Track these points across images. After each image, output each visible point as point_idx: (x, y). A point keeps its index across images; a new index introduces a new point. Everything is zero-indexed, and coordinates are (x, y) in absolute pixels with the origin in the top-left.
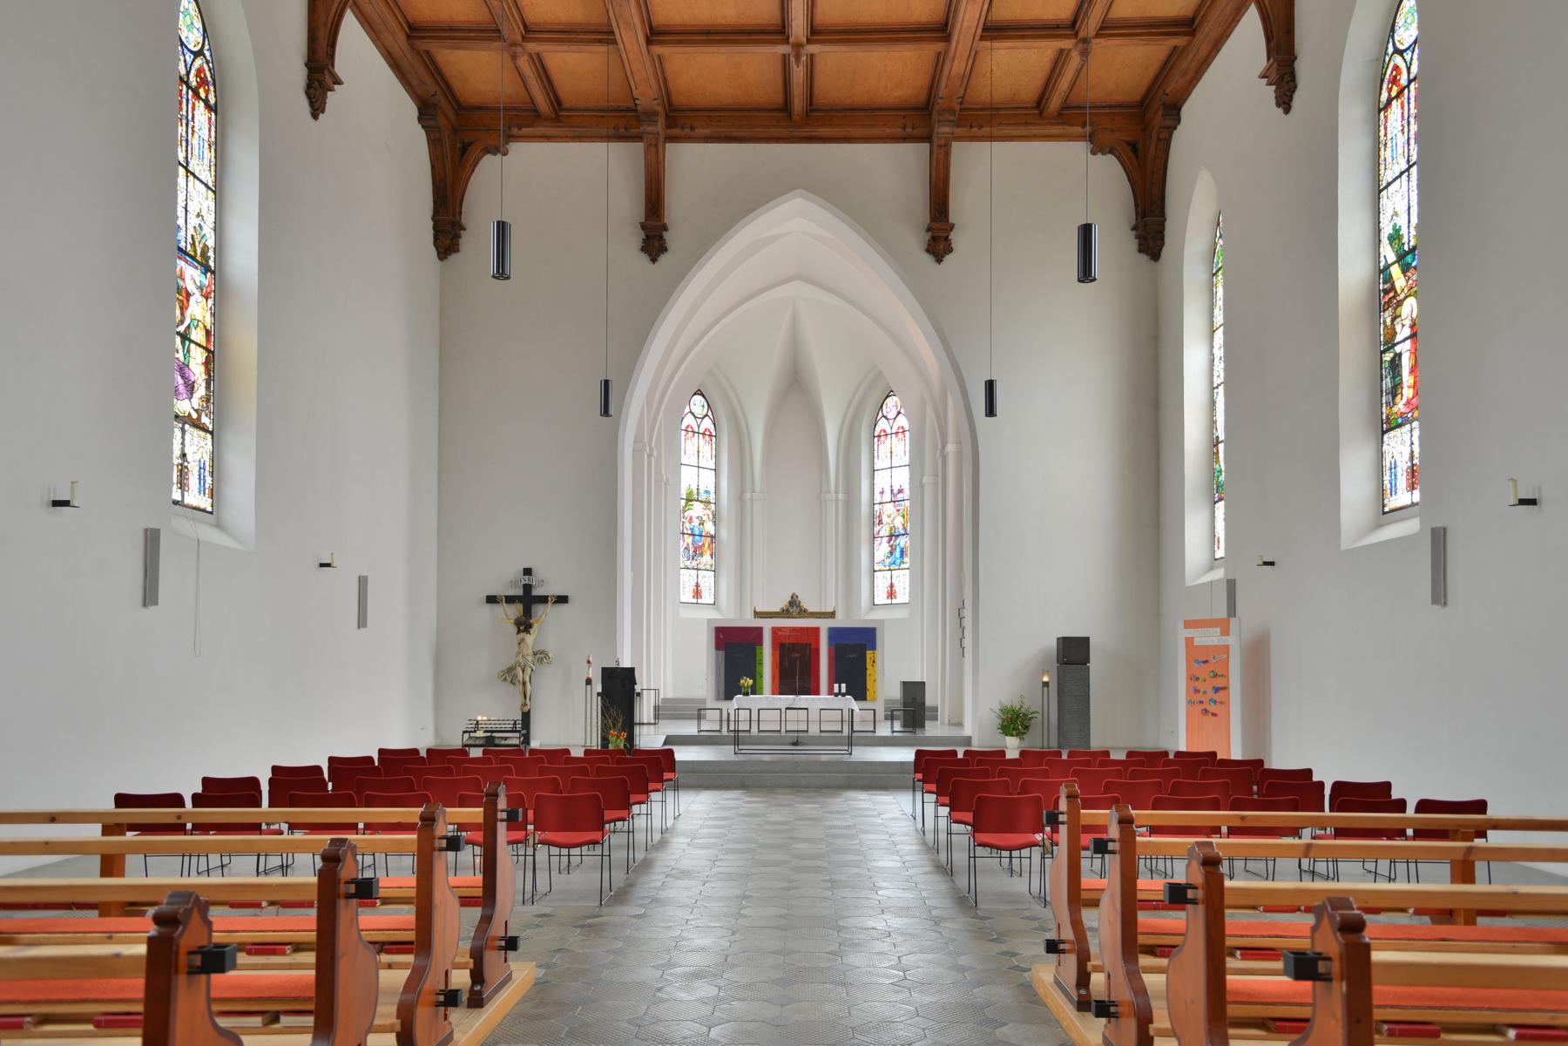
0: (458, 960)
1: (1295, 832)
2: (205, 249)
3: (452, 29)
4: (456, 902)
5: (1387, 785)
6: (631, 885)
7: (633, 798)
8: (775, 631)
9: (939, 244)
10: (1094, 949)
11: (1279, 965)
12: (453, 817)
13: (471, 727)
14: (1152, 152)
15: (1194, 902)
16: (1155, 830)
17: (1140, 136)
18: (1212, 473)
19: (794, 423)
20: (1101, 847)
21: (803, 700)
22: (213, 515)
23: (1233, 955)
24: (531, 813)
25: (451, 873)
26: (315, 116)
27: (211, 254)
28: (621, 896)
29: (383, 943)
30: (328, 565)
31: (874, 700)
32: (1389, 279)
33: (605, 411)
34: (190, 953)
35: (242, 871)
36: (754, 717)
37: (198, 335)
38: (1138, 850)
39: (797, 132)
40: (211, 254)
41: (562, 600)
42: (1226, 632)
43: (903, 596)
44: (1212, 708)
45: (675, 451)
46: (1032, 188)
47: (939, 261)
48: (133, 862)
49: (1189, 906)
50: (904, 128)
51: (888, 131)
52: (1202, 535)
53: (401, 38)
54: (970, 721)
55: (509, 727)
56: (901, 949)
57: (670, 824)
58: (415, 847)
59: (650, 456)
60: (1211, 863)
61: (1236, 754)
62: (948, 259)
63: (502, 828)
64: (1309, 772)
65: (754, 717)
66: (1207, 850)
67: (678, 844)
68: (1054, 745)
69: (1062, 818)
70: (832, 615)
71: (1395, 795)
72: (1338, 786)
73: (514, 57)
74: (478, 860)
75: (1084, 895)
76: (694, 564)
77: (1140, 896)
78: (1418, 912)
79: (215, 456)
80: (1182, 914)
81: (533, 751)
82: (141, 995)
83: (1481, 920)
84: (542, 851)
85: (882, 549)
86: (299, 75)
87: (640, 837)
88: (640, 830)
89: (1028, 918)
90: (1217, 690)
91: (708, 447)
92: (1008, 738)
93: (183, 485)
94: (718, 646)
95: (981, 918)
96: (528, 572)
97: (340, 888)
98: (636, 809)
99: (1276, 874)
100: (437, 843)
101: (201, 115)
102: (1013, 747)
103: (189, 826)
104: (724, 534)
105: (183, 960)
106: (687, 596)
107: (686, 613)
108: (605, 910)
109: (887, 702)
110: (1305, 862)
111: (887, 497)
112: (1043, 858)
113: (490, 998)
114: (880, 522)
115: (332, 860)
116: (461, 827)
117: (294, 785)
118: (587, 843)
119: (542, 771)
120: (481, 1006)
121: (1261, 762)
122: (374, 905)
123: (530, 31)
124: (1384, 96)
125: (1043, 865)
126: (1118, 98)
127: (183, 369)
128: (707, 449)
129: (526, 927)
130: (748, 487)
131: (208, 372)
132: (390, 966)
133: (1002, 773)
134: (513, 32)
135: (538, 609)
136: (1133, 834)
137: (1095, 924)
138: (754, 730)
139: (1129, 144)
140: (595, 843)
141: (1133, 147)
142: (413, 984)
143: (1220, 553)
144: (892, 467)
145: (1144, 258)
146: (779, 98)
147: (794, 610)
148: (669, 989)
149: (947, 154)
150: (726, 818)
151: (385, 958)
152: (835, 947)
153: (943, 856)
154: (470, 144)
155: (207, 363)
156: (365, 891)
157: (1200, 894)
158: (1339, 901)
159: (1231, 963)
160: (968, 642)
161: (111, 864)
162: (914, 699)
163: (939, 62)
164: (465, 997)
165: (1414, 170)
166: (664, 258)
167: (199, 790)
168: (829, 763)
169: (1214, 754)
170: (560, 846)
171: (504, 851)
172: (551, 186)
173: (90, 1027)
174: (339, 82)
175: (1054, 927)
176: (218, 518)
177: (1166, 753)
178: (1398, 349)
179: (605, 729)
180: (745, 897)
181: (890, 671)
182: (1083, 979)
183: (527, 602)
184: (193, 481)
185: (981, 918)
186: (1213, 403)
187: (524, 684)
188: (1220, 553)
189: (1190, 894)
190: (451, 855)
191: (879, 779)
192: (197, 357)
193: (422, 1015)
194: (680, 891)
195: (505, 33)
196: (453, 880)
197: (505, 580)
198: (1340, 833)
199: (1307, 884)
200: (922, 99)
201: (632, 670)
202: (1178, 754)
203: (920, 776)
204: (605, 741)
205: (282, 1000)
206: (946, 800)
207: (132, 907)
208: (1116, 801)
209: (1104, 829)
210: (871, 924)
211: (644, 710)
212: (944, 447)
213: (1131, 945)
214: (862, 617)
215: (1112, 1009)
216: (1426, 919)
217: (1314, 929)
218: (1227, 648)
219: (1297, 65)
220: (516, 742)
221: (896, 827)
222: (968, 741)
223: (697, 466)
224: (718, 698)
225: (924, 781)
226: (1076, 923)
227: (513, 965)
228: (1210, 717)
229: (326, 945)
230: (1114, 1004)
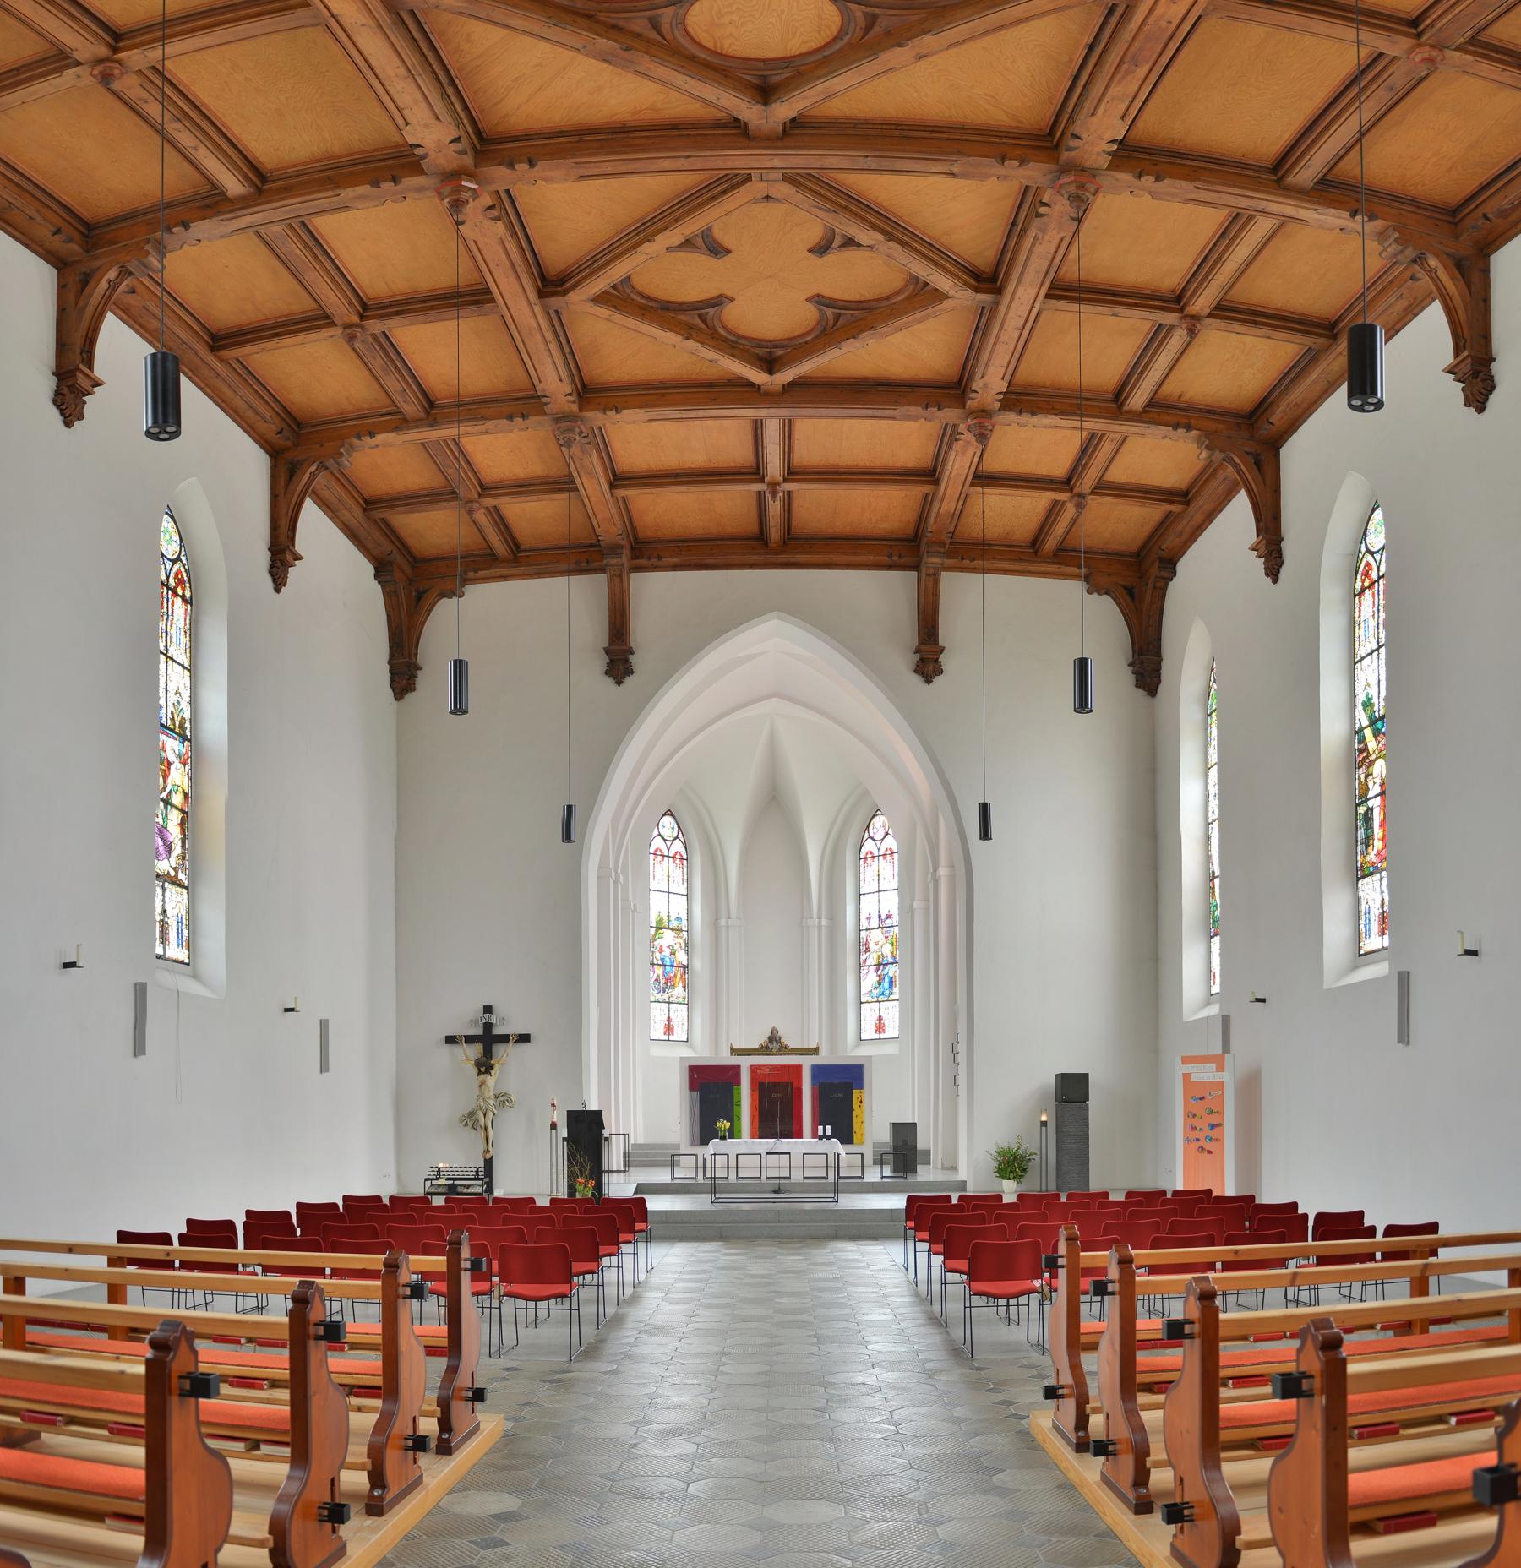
0: (425, 1407)
1: (1282, 1263)
2: (183, 720)
3: (407, 497)
4: (422, 1352)
5: (1360, 1214)
6: (602, 1341)
7: (603, 1249)
8: (754, 1069)
9: (928, 664)
10: (1093, 1390)
11: (1268, 1389)
12: (417, 1264)
13: (433, 1175)
15: (1191, 1336)
16: (1153, 1270)
19: (772, 841)
20: (1101, 1289)
21: (785, 1144)
22: (189, 966)
23: (1225, 1385)
24: (495, 1265)
25: (416, 1322)
26: (278, 590)
27: (187, 725)
28: (591, 1352)
29: (353, 1386)
31: (862, 1143)
32: (1363, 740)
34: (181, 1377)
35: (223, 1308)
36: (732, 1163)
37: (177, 799)
38: (1137, 1290)
39: (772, 558)
40: (187, 725)
41: (524, 1038)
42: (1221, 1068)
43: (892, 1030)
44: (1208, 1145)
45: (643, 875)
48: (133, 1292)
49: (1186, 1341)
50: (890, 556)
51: (872, 558)
52: (1198, 969)
54: (965, 1165)
55: (472, 1174)
56: (893, 1404)
57: (642, 1277)
58: (380, 1294)
60: (1207, 1297)
61: (1230, 1191)
62: (938, 680)
63: (466, 1278)
64: (1295, 1205)
65: (732, 1163)
66: (1204, 1285)
67: (652, 1298)
68: (1052, 1188)
69: (1061, 1261)
70: (815, 1051)
71: (1367, 1223)
72: (1320, 1217)
73: (470, 512)
74: (443, 1310)
75: (1083, 1339)
76: (666, 996)
77: (1139, 1336)
78: (1384, 1328)
79: (190, 910)
80: (1179, 1352)
81: (496, 1200)
82: (143, 1411)
83: (1433, 1329)
84: (508, 1304)
85: (869, 979)
86: (263, 558)
87: (611, 1291)
88: (610, 1284)
89: (1025, 1366)
90: (1213, 1127)
91: (679, 871)
92: (1005, 1182)
93: (164, 940)
94: (692, 1087)
95: (977, 1369)
96: (488, 1009)
97: (310, 1332)
98: (605, 1261)
99: (1267, 1302)
100: (401, 1291)
101: (179, 607)
102: (1009, 1191)
103: (177, 1264)
104: (697, 964)
105: (175, 1381)
106: (658, 1032)
107: (657, 1051)
108: (574, 1365)
109: (875, 1145)
110: (1291, 1290)
111: (875, 923)
112: (1041, 1305)
113: (458, 1447)
114: (867, 950)
115: (301, 1302)
116: (426, 1275)
117: (266, 1228)
118: (556, 1296)
119: (506, 1221)
120: (450, 1453)
121: (1252, 1198)
122: (342, 1349)
123: (485, 489)
124: (1358, 585)
125: (1041, 1313)
127: (162, 832)
128: (678, 873)
129: (493, 1380)
130: (724, 913)
131: (183, 831)
132: (359, 1409)
133: (998, 1219)
134: (469, 490)
135: (499, 1050)
136: (1133, 1274)
137: (1094, 1368)
138: (732, 1177)
139: (1125, 588)
140: (563, 1296)
141: (1130, 591)
142: (382, 1427)
143: (1216, 989)
144: (879, 891)
145: (1141, 692)
147: (775, 1046)
148: (644, 1445)
149: (937, 583)
150: (704, 1272)
151: (355, 1401)
152: (821, 1403)
153: (937, 1308)
155: (182, 824)
156: (333, 1333)
157: (1196, 1328)
158: (1321, 1322)
159: (1224, 1393)
160: (962, 1080)
161: (116, 1293)
162: (905, 1142)
163: (926, 504)
164: (433, 1444)
165: (1383, 650)
166: (629, 681)
167: (184, 1231)
168: (816, 1211)
169: (1210, 1191)
170: (527, 1299)
171: (469, 1303)
172: (515, 625)
173: (106, 1433)
175: (1053, 1374)
176: (194, 969)
177: (1164, 1193)
178: (1370, 804)
179: (572, 1177)
180: (725, 1354)
181: (877, 1116)
182: (1082, 1422)
183: (487, 1042)
184: (173, 935)
185: (977, 1369)
187: (486, 1129)
188: (1216, 989)
189: (1187, 1329)
190: (415, 1302)
191: (867, 1228)
192: (175, 817)
193: (392, 1458)
194: (654, 1348)
195: (461, 492)
196: (418, 1329)
197: (465, 1021)
198: (1322, 1260)
199: (1293, 1310)
200: (910, 530)
201: (600, 1112)
202: (1176, 1193)
203: (912, 1224)
204: (572, 1189)
205: (261, 1429)
206: (940, 1248)
207: (133, 1333)
208: (1115, 1241)
209: (1104, 1271)
210: (860, 1379)
211: (614, 1156)
212: (935, 870)
213: (1130, 1384)
214: (849, 1054)
215: (1111, 1448)
216: (1390, 1333)
217: (1299, 1350)
218: (1221, 1085)
220: (479, 1190)
221: (885, 1283)
222: (963, 1185)
223: (668, 892)
224: (692, 1143)
225: (916, 1229)
226: (1076, 1368)
227: (480, 1416)
228: (1206, 1154)
229: (299, 1382)
230: (1112, 1442)
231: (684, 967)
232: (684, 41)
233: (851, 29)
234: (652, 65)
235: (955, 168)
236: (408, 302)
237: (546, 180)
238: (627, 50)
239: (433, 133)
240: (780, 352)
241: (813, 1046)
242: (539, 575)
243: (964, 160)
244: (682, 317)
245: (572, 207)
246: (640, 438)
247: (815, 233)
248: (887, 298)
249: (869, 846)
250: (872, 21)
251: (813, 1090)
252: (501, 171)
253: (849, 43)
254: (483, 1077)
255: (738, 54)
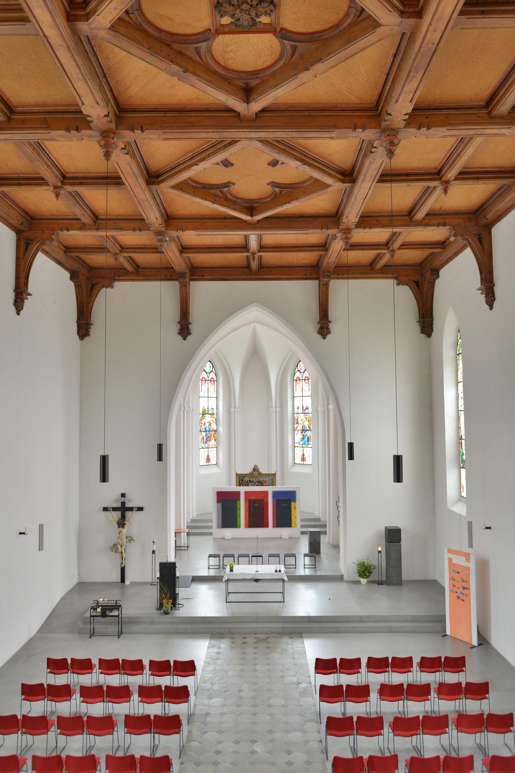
3: (86, 248)
8: (246, 493)
9: (324, 330)
14: (426, 288)
17: (421, 279)
18: (459, 454)
30: (24, 533)
33: (160, 458)
39: (252, 277)
41: (141, 509)
43: (309, 461)
44: (462, 597)
46: (371, 305)
47: (324, 338)
50: (306, 275)
53: (62, 253)
59: (184, 411)
62: (329, 337)
76: (207, 445)
85: (299, 436)
86: (11, 295)
90: (464, 588)
94: (218, 502)
96: (123, 495)
104: (221, 430)
106: (203, 462)
111: (301, 411)
126: (408, 262)
130: (233, 406)
135: (128, 514)
139: (415, 282)
141: (417, 283)
144: (303, 397)
145: (423, 336)
146: (244, 243)
147: (256, 473)
154: (95, 284)
160: (341, 519)
162: (315, 540)
166: (189, 338)
172: (135, 305)
174: (30, 295)
186: (459, 418)
187: (122, 553)
197: (114, 502)
200: (315, 262)
219: (495, 288)
231: (215, 431)
232: (210, 61)
233: (285, 56)
234: (197, 81)
235: (333, 135)
236: (85, 178)
237: (150, 139)
238: (185, 72)
239: (95, 109)
240: (256, 205)
241: (273, 472)
242: (148, 280)
243: (337, 131)
244: (212, 191)
245: (162, 147)
246: (191, 237)
247: (270, 159)
248: (303, 182)
249: (298, 374)
250: (294, 49)
251: (273, 502)
252: (128, 133)
253: (284, 64)
254: (121, 529)
255: (235, 68)
